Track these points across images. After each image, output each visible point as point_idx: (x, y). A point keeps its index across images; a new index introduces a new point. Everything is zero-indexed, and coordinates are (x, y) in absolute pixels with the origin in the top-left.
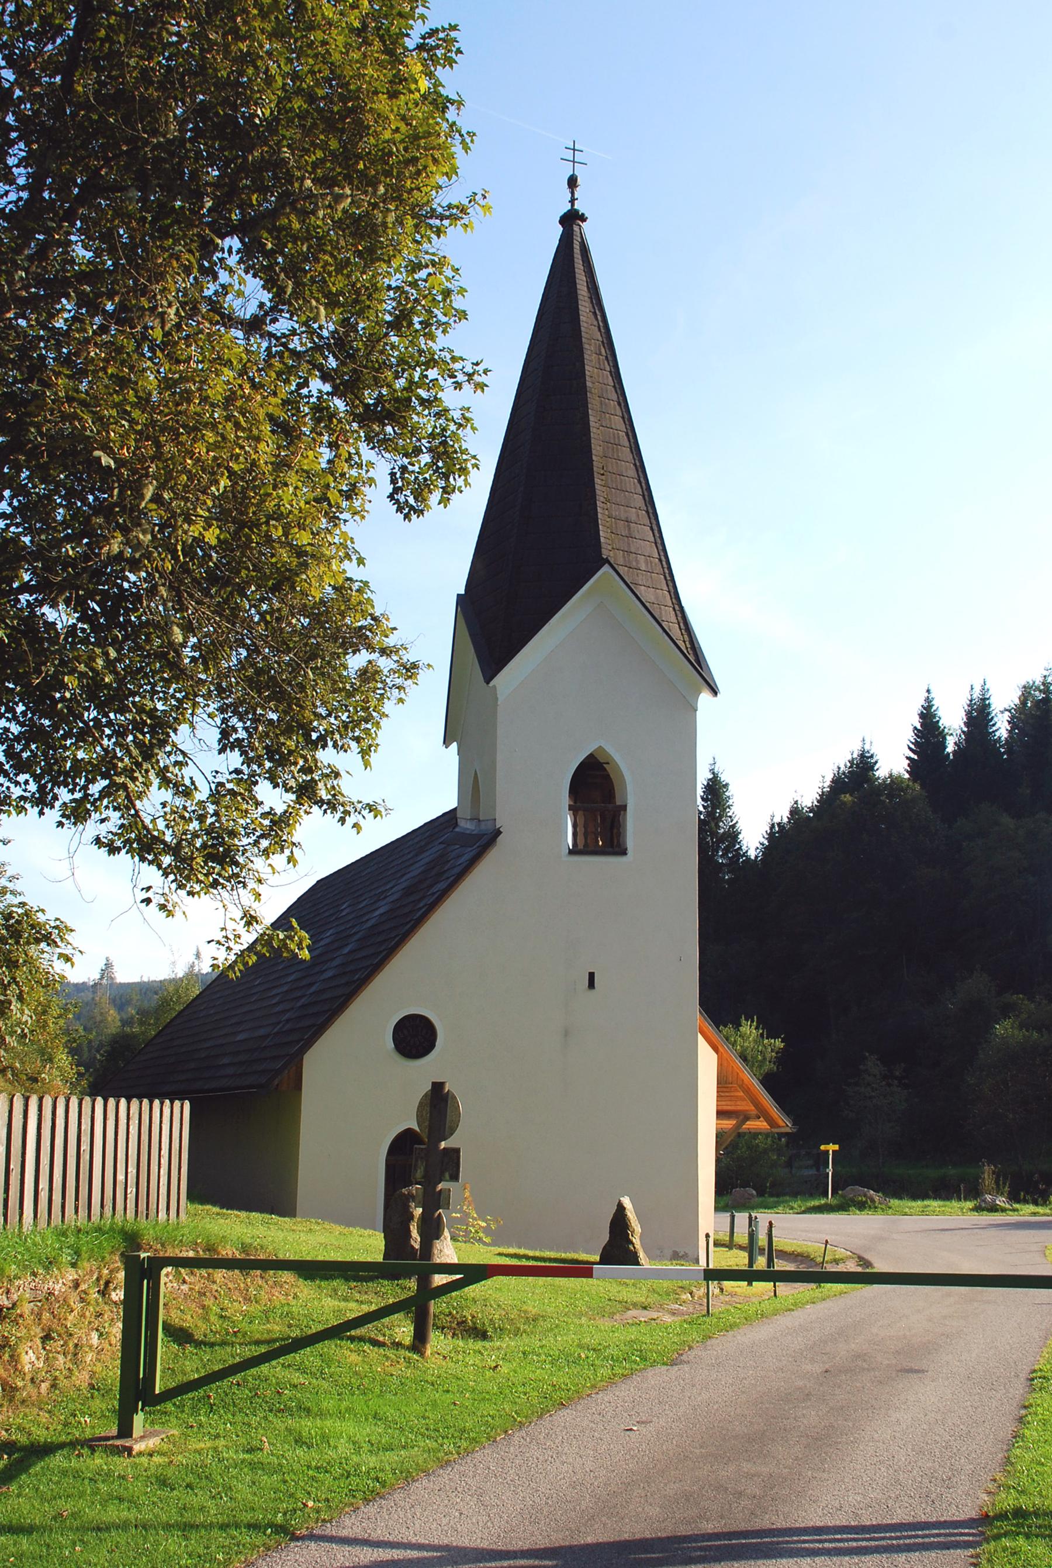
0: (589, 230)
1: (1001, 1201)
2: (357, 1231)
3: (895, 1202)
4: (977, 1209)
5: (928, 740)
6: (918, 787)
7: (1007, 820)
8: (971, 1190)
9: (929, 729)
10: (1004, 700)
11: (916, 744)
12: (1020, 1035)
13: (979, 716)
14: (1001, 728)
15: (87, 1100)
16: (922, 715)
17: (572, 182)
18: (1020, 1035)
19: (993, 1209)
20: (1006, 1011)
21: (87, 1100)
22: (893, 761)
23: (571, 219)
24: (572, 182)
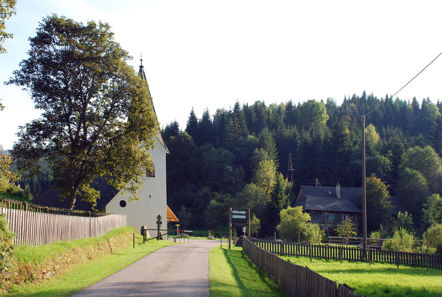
0: (144, 69)
1: (213, 238)
2: (404, 275)
3: (191, 237)
4: (208, 239)
5: (192, 121)
6: (191, 137)
7: (213, 149)
8: (207, 236)
9: (193, 118)
10: (212, 114)
11: (189, 121)
12: (217, 203)
13: (206, 116)
14: (212, 119)
15: (12, 210)
16: (191, 114)
17: (141, 60)
18: (217, 203)
19: (211, 239)
20: (214, 197)
21: (17, 210)
22: (183, 127)
23: (141, 67)
24: (141, 60)
